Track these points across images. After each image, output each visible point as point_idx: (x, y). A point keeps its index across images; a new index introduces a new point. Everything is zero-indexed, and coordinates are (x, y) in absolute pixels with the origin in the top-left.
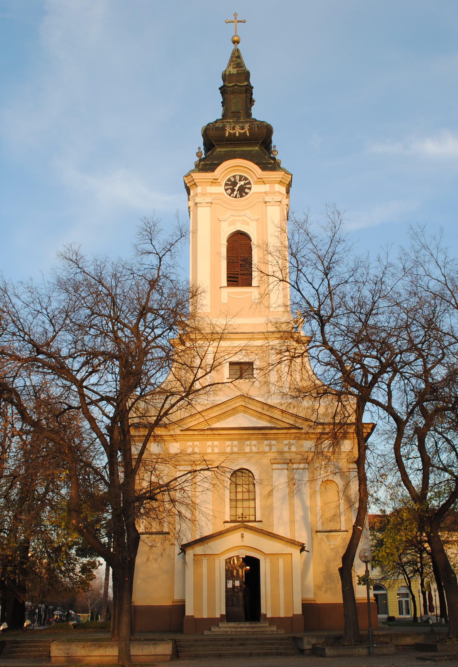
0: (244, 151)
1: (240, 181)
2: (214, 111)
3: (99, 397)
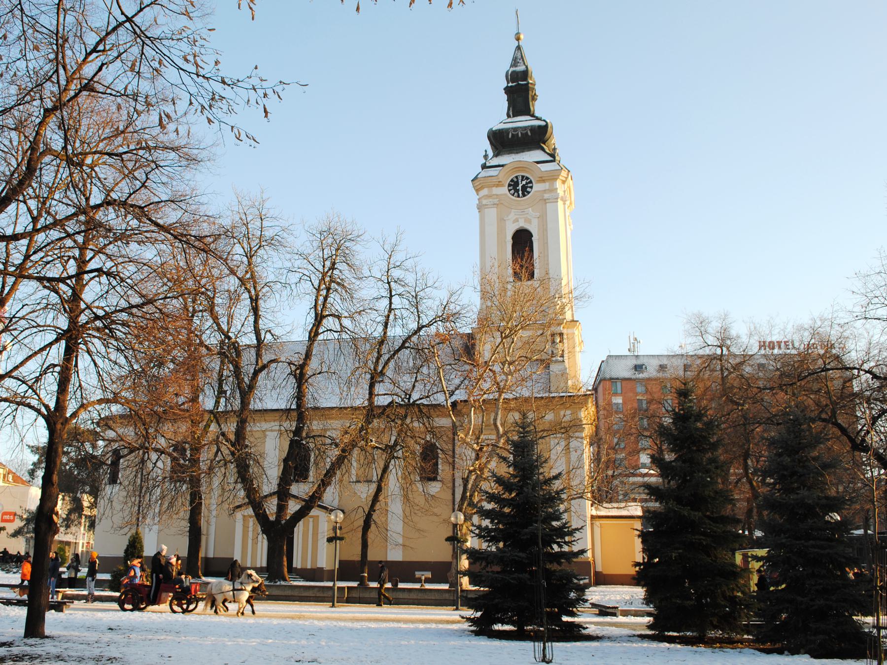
0: (370, 628)
1: (522, 180)
2: (497, 114)
3: (13, 374)
